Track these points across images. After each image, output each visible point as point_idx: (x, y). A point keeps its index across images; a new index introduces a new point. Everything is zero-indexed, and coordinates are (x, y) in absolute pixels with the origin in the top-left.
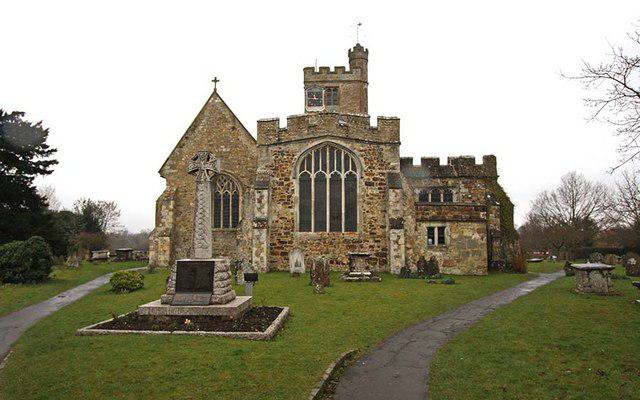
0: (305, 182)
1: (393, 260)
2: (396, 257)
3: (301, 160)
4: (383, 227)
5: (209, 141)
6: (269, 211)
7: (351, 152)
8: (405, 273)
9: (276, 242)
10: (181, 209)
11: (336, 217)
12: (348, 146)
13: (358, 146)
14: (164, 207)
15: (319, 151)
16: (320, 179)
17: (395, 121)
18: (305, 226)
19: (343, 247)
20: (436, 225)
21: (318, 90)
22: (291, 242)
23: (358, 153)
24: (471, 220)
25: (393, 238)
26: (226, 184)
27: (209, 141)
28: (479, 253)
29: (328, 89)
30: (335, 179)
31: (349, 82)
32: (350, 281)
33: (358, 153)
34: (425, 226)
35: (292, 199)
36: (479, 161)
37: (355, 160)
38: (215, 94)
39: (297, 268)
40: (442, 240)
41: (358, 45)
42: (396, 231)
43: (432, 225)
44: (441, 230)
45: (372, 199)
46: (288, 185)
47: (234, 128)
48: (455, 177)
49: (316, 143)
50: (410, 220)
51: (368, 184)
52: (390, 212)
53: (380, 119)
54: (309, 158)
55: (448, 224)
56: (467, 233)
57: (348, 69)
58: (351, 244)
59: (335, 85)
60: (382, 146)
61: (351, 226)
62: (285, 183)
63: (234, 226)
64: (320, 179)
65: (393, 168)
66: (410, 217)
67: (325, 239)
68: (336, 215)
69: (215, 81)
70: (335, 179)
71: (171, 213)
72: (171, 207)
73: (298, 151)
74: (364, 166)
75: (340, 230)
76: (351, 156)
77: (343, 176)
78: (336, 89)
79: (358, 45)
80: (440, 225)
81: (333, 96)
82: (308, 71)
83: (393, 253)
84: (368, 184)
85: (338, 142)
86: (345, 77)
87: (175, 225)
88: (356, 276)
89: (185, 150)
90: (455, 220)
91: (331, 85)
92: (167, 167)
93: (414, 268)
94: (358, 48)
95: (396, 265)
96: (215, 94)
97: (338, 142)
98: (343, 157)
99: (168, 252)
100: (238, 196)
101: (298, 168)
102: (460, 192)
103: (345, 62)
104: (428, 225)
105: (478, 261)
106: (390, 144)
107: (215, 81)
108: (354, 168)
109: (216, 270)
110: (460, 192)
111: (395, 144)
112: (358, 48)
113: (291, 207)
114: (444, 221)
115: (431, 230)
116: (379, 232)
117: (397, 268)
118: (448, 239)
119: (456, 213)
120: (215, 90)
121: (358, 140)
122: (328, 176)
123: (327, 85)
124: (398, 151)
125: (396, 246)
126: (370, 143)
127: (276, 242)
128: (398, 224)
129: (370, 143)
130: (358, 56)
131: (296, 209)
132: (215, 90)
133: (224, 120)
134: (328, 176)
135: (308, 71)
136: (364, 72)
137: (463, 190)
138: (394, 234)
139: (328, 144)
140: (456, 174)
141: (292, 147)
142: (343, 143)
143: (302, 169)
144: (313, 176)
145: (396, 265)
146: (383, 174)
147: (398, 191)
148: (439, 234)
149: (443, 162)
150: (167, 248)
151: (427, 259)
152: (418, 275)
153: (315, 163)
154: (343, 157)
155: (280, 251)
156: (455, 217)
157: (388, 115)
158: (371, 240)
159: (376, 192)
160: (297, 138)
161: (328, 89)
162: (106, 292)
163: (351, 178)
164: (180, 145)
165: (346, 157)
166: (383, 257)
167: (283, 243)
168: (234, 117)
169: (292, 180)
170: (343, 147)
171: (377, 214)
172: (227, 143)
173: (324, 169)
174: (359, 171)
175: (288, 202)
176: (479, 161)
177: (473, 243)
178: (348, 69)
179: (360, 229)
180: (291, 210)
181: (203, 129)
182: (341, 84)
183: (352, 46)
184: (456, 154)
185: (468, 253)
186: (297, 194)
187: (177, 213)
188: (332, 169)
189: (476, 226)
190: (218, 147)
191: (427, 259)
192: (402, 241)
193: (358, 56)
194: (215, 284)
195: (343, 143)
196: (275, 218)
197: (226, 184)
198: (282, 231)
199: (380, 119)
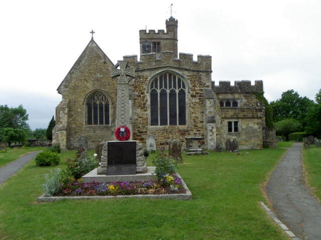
0: (154, 95)
1: (209, 141)
2: (211, 140)
3: (151, 82)
4: (202, 122)
5: (89, 70)
6: (133, 113)
7: (182, 76)
8: (218, 149)
9: (137, 132)
10: (72, 113)
11: (173, 116)
12: (180, 73)
13: (186, 73)
14: (61, 112)
15: (163, 76)
16: (163, 94)
17: (208, 58)
18: (154, 122)
19: (178, 134)
20: (233, 121)
21: (148, 44)
22: (146, 132)
23: (187, 78)
24: (253, 118)
25: (209, 128)
26: (100, 97)
27: (89, 70)
28: (258, 136)
29: (154, 43)
30: (173, 94)
31: (167, 39)
32: (190, 154)
33: (187, 78)
34: (226, 121)
35: (146, 105)
36: (253, 84)
37: (184, 82)
38: (92, 41)
39: (151, 148)
40: (236, 130)
41: (171, 17)
42: (211, 124)
43: (231, 120)
44: (236, 123)
45: (195, 105)
46: (144, 97)
47: (105, 63)
48: (239, 93)
49: (160, 71)
50: (218, 118)
51: (193, 96)
52: (207, 113)
53: (199, 57)
54: (156, 80)
55: (240, 120)
56: (251, 125)
57: (165, 32)
58: (183, 133)
59: (158, 41)
60: (200, 73)
61: (183, 122)
62: (142, 96)
63: (106, 124)
64: (163, 94)
65: (208, 87)
66: (218, 116)
67: (167, 130)
68: (173, 115)
69: (92, 32)
70: (173, 94)
71: (66, 116)
72: (66, 112)
73: (149, 75)
74: (190, 85)
75: (176, 124)
76: (182, 79)
77: (177, 91)
78: (159, 43)
79: (171, 17)
80: (235, 120)
81: (157, 46)
82: (142, 32)
83: (209, 138)
84: (193, 96)
85: (174, 70)
86: (165, 36)
87: (69, 123)
88: (193, 151)
89: (74, 76)
90: (244, 118)
91: (156, 41)
92: (62, 87)
93: (224, 146)
94: (172, 19)
95: (211, 143)
96: (92, 41)
97: (174, 70)
98: (177, 80)
99: (65, 140)
100: (108, 105)
101: (150, 87)
102: (242, 101)
103: (164, 27)
104: (228, 120)
105: (257, 141)
106: (206, 72)
107: (92, 32)
108: (184, 87)
109: (137, 148)
110: (242, 101)
111: (208, 72)
112: (172, 19)
113: (145, 111)
114: (238, 118)
115: (230, 123)
116: (200, 125)
117: (212, 146)
118: (240, 129)
119: (245, 113)
120: (92, 38)
121: (186, 70)
122: (168, 91)
123: (154, 41)
124: (210, 76)
125: (211, 133)
126: (194, 71)
127: (137, 132)
128: (212, 120)
129: (194, 71)
130: (172, 24)
131: (149, 112)
132: (92, 38)
133: (99, 57)
134: (168, 91)
135: (142, 32)
136: (175, 33)
137: (244, 100)
138: (209, 126)
139: (167, 72)
140: (240, 91)
141: (146, 74)
142: (177, 71)
143: (152, 87)
144: (159, 91)
145: (211, 143)
146: (202, 90)
147: (212, 100)
148: (235, 126)
149: (232, 84)
150: (64, 138)
151: (232, 141)
152: (227, 149)
153: (160, 84)
154: (177, 80)
155: (139, 138)
156: (244, 115)
157: (204, 54)
158: (195, 130)
159: (197, 101)
160: (149, 67)
161: (154, 43)
162: (30, 167)
163: (182, 93)
164: (70, 73)
165: (179, 80)
166: (202, 141)
167: (141, 132)
168: (105, 56)
169: (146, 94)
170: (177, 74)
171: (198, 115)
172: (101, 71)
173: (166, 87)
174: (187, 88)
175: (143, 107)
176: (253, 84)
177: (254, 131)
178: (165, 32)
179: (187, 123)
180: (146, 113)
181: (85, 63)
182: (161, 41)
183: (168, 18)
184: (240, 79)
185: (252, 136)
186: (149, 103)
187: (70, 116)
188: (170, 87)
189: (256, 121)
190: (95, 74)
191: (232, 141)
192: (214, 130)
193: (172, 24)
194: (137, 158)
195: (177, 71)
196: (136, 117)
197: (100, 97)
198: (140, 125)
199: (199, 57)
